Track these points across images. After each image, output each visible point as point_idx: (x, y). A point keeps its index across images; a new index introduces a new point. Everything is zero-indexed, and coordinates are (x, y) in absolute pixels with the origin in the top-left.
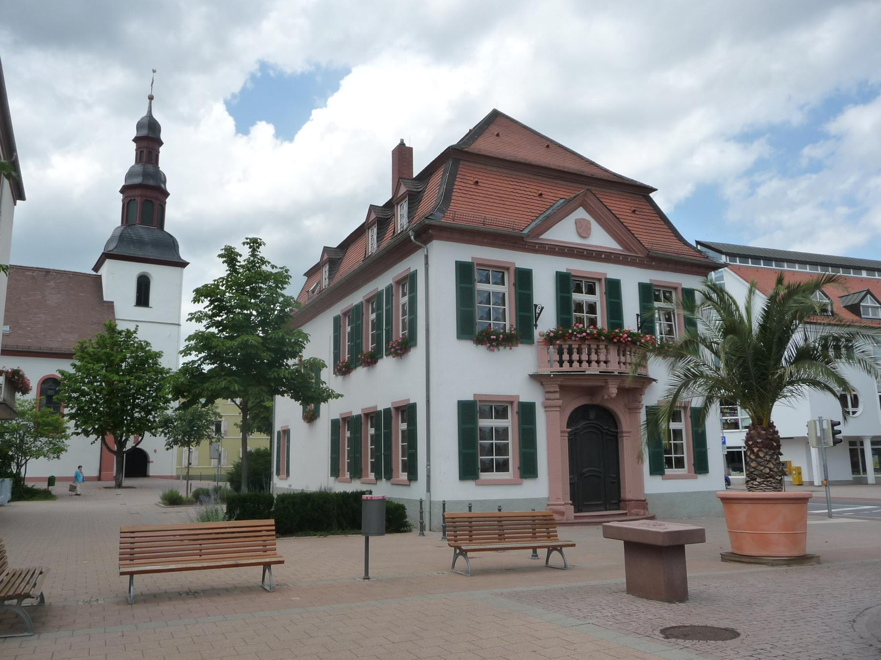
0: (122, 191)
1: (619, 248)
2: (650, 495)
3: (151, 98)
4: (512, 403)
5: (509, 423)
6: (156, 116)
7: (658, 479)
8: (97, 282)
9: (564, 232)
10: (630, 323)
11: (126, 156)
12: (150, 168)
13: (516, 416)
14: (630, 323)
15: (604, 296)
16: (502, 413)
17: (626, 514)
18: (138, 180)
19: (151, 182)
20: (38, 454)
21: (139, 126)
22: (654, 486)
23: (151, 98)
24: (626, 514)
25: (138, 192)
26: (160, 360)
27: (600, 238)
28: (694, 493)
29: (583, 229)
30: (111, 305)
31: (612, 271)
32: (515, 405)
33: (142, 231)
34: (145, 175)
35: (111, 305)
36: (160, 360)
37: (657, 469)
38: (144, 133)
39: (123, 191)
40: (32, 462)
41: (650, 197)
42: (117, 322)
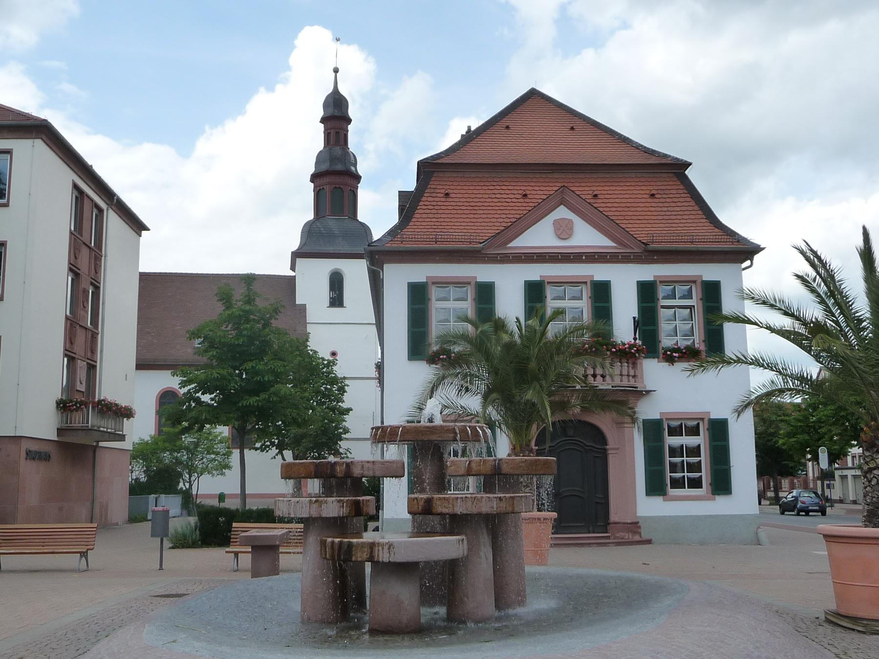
0: (312, 181)
1: (611, 243)
2: (640, 517)
3: (336, 71)
4: (702, 419)
5: (701, 440)
6: (342, 90)
7: (657, 501)
8: (289, 284)
9: (540, 236)
10: (623, 330)
11: (313, 140)
12: (338, 151)
13: (707, 433)
14: (623, 330)
15: (590, 301)
16: (694, 431)
17: (608, 538)
18: (324, 167)
19: (339, 167)
20: (205, 470)
21: (326, 105)
22: (649, 508)
23: (336, 71)
24: (608, 538)
25: (326, 180)
26: (334, 368)
27: (587, 237)
28: (711, 516)
29: (563, 230)
30: (303, 308)
31: (600, 272)
32: (706, 421)
33: (331, 223)
34: (333, 159)
35: (303, 308)
36: (334, 368)
37: (655, 487)
38: (331, 111)
39: (314, 178)
40: (205, 478)
41: (686, 177)
42: (310, 329)
